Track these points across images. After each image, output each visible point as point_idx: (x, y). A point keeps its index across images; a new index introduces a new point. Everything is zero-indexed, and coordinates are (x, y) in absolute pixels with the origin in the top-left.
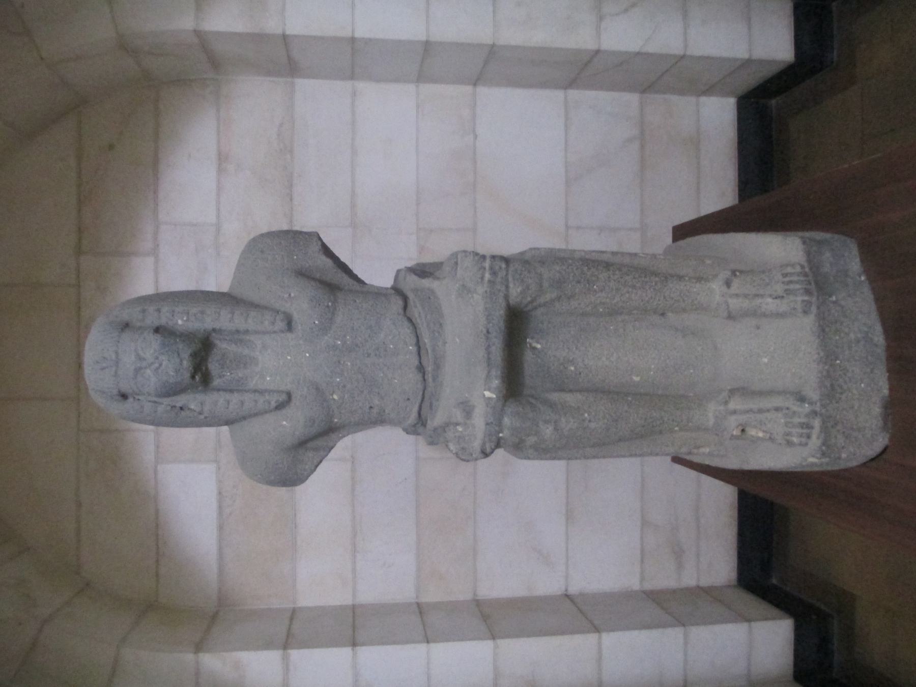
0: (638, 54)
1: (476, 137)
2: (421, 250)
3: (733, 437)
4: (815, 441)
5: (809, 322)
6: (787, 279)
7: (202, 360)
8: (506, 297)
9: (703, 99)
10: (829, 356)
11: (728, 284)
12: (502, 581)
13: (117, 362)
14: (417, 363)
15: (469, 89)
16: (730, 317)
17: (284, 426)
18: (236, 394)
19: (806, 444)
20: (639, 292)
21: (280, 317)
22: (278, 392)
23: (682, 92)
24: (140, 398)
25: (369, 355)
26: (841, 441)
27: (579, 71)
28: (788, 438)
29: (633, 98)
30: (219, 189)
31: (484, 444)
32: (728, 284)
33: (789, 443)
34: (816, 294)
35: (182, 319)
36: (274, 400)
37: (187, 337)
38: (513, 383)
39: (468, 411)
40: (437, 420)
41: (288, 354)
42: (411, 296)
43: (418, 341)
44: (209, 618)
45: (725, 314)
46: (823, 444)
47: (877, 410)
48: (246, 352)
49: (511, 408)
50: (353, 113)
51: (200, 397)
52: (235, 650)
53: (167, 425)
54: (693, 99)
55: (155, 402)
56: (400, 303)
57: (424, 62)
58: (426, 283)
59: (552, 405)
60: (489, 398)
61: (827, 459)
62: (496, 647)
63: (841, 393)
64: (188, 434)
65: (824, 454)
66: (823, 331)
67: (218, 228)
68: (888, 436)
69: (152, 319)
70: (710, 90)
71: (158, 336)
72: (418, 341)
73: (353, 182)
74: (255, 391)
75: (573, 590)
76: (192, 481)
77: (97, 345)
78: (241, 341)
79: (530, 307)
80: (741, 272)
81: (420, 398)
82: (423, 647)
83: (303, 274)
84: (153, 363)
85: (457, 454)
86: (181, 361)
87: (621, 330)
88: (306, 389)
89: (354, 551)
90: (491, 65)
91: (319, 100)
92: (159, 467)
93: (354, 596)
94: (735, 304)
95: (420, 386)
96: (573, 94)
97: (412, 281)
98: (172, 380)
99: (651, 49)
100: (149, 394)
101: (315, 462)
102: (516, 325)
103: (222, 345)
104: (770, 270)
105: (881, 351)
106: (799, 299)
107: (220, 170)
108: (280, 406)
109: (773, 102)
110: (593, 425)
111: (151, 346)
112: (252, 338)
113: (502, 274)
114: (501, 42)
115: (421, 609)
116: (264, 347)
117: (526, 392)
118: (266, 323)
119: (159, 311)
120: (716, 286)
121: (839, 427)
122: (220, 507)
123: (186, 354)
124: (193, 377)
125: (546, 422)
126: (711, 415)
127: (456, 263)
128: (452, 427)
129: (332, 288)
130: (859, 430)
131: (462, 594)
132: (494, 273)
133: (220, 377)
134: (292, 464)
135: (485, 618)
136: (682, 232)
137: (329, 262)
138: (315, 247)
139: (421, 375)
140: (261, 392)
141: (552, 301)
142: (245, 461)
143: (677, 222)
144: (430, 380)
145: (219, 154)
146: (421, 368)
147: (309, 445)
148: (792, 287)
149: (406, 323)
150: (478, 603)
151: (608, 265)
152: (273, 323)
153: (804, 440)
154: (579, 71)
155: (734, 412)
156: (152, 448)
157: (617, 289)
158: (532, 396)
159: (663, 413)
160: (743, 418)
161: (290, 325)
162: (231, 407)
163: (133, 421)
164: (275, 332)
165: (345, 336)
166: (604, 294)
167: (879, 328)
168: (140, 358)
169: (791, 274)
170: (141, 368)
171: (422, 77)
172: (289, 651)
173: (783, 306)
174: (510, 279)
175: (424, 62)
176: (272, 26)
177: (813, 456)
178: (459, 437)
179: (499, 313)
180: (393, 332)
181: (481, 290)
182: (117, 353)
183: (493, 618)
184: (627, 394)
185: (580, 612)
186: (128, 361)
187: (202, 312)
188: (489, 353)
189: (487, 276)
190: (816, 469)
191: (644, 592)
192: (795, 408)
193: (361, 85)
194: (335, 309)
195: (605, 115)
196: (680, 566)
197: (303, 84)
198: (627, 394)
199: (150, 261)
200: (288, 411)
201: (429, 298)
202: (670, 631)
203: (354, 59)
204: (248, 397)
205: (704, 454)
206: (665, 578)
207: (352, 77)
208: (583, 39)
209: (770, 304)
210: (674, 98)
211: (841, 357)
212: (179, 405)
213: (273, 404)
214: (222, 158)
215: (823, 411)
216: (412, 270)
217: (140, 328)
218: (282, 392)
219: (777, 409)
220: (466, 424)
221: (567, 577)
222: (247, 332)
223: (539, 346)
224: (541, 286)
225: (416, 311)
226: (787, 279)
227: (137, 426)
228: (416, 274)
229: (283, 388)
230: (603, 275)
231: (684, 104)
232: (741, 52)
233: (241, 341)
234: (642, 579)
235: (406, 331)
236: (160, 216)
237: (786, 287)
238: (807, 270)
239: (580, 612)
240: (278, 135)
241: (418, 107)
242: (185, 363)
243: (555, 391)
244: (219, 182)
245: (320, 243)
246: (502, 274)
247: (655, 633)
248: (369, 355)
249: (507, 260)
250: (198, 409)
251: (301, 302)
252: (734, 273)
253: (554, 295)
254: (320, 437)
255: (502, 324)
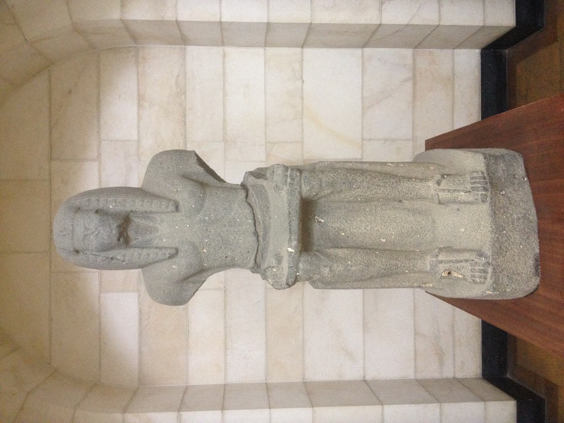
0: (407, 25)
1: (303, 82)
2: (268, 155)
3: (442, 278)
4: (489, 281)
5: (486, 207)
6: (473, 181)
7: (124, 229)
8: (300, 193)
9: (457, 51)
10: (498, 229)
11: (439, 183)
12: (322, 370)
13: (73, 231)
14: (254, 230)
15: (299, 50)
16: (440, 203)
17: (174, 269)
18: (145, 250)
19: (484, 283)
20: (382, 189)
21: (171, 203)
22: (170, 248)
23: (442, 47)
24: (88, 252)
25: (225, 226)
26: (506, 281)
27: (370, 37)
28: (474, 278)
29: (408, 52)
30: (139, 118)
31: (288, 279)
32: (439, 183)
33: (475, 282)
34: (490, 190)
35: (112, 205)
36: (168, 253)
37: (115, 215)
38: (306, 243)
39: (279, 260)
40: (264, 266)
41: (177, 225)
42: (251, 190)
43: (254, 217)
44: (136, 391)
45: (437, 202)
46: (494, 283)
47: (531, 262)
48: (151, 224)
49: (304, 258)
50: (224, 68)
51: (123, 252)
52: (148, 412)
53: (104, 268)
54: (450, 51)
55: (96, 255)
56: (244, 194)
57: (267, 35)
58: (260, 181)
59: (328, 256)
60: (290, 252)
61: (498, 292)
62: (314, 412)
63: (506, 252)
64: (121, 274)
65: (494, 289)
66: (495, 213)
67: (139, 141)
68: (539, 278)
69: (94, 205)
70: (460, 46)
71: (97, 216)
72: (254, 217)
73: (224, 113)
74: (157, 248)
75: (369, 377)
76: (122, 304)
77: (61, 221)
78: (148, 217)
79: (315, 198)
80: (448, 175)
81: (255, 252)
82: (266, 411)
83: (186, 177)
84: (94, 231)
85: (273, 285)
86: (112, 230)
87: (374, 211)
88: (187, 246)
89: (226, 348)
90: (311, 36)
91: (202, 60)
92: (102, 295)
93: (225, 378)
94: (443, 195)
95: (256, 245)
96: (367, 51)
97: (252, 180)
98: (106, 242)
99: (416, 22)
100: (92, 251)
101: (194, 291)
102: (307, 209)
103: (137, 220)
104: (465, 175)
105: (535, 225)
106: (480, 193)
107: (140, 106)
108: (171, 257)
109: (507, 51)
110: (353, 268)
111: (93, 221)
112: (155, 216)
113: (297, 179)
114: (316, 21)
115: (268, 387)
116: (162, 221)
117: (315, 248)
118: (163, 207)
119: (98, 200)
120: (431, 184)
121: (505, 272)
122: (140, 320)
123: (114, 226)
124: (119, 240)
125: (325, 266)
126: (428, 263)
127: (273, 172)
128: (270, 269)
129: (203, 185)
130: (518, 274)
131: (295, 377)
132: (293, 179)
133: (136, 240)
134: (180, 291)
135: (309, 394)
136: (434, 144)
137: (201, 170)
138: (194, 160)
139: (256, 238)
140: (160, 248)
141: (329, 195)
142: (152, 291)
143: (430, 136)
144: (262, 240)
145: (139, 95)
146: (256, 233)
147: (190, 280)
148: (476, 185)
149: (247, 206)
150: (305, 384)
151: (363, 172)
152: (167, 207)
153: (482, 280)
154: (370, 37)
155: (441, 262)
156: (97, 283)
157: (368, 187)
158: (318, 251)
159: (397, 262)
160: (447, 266)
161: (177, 208)
162: (142, 257)
163: (83, 266)
164: (168, 212)
165: (210, 214)
166: (360, 190)
167: (533, 211)
168: (86, 229)
169: (476, 178)
170: (87, 235)
171: (266, 44)
172: (182, 413)
173: (471, 198)
174: (303, 182)
175: (267, 35)
176: (169, 16)
177: (488, 290)
178: (274, 275)
179: (296, 202)
180: (239, 211)
181: (285, 188)
182: (73, 225)
183: (313, 393)
184: (376, 250)
185: (372, 392)
186: (80, 230)
187: (125, 200)
188: (290, 226)
189: (289, 180)
190: (490, 298)
191: (417, 380)
192: (476, 260)
193: (228, 49)
194: (204, 198)
195: (388, 62)
196: (442, 364)
197: (191, 49)
198: (376, 250)
199: (96, 164)
200: (175, 259)
201: (261, 192)
202: (430, 406)
203: (223, 34)
204: (152, 252)
205: (429, 287)
206: (431, 371)
207: (223, 44)
208: (370, 17)
209: (463, 196)
210: (437, 52)
211: (507, 229)
212: (111, 256)
213: (167, 256)
214: (141, 98)
215: (494, 262)
216: (251, 173)
217: (87, 210)
218: (173, 248)
219: (466, 261)
220: (278, 267)
221: (364, 368)
222: (151, 212)
223: (323, 221)
224: (321, 185)
225: (253, 199)
226: (473, 181)
227: (86, 269)
228: (254, 177)
229: (174, 245)
230: (359, 179)
231: (443, 56)
232: (477, 21)
233: (148, 217)
234: (416, 371)
235: (247, 211)
236: (101, 136)
237: (473, 186)
238: (486, 175)
239: (372, 392)
240: (176, 83)
241: (265, 63)
242: (114, 231)
243: (331, 248)
244: (138, 114)
245: (196, 158)
246: (297, 179)
247: (421, 406)
248: (225, 226)
249: (300, 171)
250: (122, 259)
251: (184, 194)
252: (443, 176)
253: (329, 191)
254: (196, 275)
255: (298, 209)
